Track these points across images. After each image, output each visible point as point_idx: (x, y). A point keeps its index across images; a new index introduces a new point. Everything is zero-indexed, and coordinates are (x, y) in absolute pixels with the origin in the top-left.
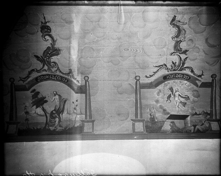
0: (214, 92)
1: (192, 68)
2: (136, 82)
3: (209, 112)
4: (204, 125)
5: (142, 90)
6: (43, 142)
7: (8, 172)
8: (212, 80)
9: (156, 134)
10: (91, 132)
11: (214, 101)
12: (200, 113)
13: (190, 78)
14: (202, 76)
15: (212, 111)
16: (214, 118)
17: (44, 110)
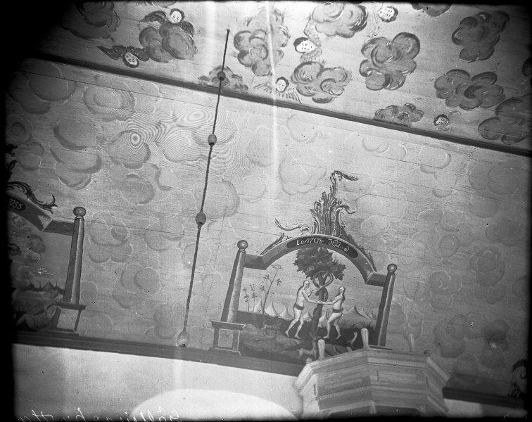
0: (78, 245)
1: (28, 186)
2: (239, 252)
3: (62, 287)
4: (43, 314)
5: (245, 269)
6: (63, 349)
7: (22, 414)
8: (76, 219)
9: (396, 374)
10: (72, 331)
11: (76, 264)
12: (42, 287)
13: (24, 207)
14: (53, 208)
15: (69, 284)
16: (73, 301)
17: (263, 307)
